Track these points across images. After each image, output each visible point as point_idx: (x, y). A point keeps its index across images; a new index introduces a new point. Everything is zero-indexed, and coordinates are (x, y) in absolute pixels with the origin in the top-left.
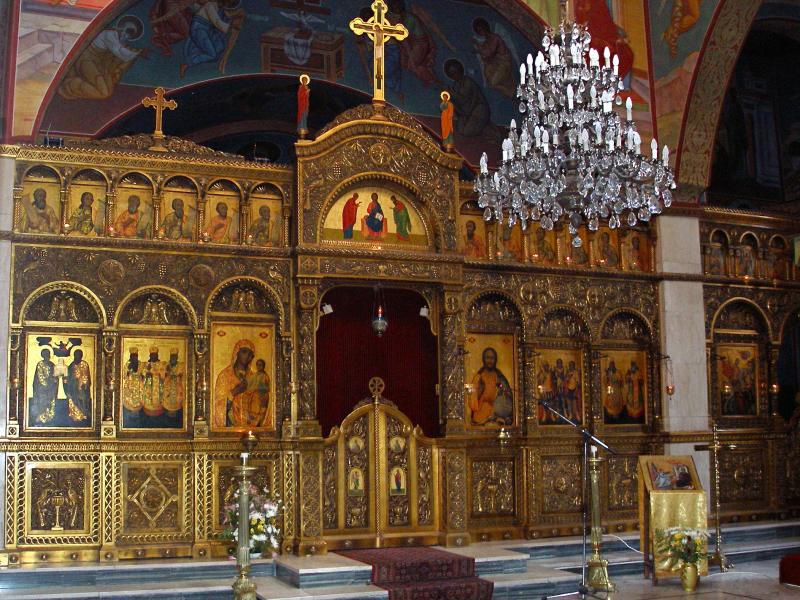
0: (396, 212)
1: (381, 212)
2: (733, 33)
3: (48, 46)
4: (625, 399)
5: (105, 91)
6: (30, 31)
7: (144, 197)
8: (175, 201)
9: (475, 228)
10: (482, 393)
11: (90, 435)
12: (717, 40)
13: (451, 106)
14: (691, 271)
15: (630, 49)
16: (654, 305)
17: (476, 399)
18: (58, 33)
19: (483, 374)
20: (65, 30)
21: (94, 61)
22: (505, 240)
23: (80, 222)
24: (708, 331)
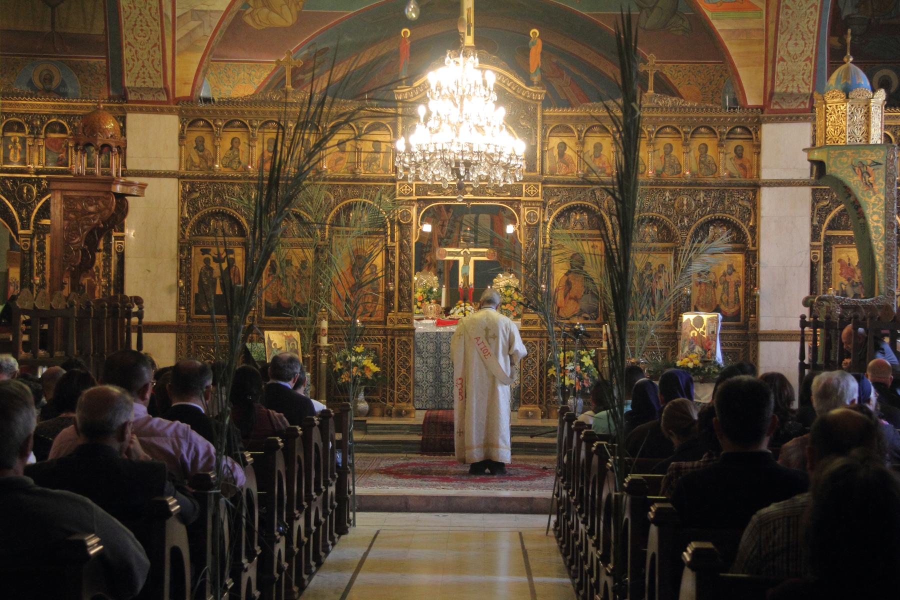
3: (200, 22)
4: (718, 299)
6: (186, 11)
7: (244, 140)
10: (569, 291)
13: (539, 42)
14: (796, 176)
16: (754, 208)
17: (563, 297)
18: (206, 11)
19: (570, 276)
20: (212, 8)
22: (595, 157)
24: (815, 236)
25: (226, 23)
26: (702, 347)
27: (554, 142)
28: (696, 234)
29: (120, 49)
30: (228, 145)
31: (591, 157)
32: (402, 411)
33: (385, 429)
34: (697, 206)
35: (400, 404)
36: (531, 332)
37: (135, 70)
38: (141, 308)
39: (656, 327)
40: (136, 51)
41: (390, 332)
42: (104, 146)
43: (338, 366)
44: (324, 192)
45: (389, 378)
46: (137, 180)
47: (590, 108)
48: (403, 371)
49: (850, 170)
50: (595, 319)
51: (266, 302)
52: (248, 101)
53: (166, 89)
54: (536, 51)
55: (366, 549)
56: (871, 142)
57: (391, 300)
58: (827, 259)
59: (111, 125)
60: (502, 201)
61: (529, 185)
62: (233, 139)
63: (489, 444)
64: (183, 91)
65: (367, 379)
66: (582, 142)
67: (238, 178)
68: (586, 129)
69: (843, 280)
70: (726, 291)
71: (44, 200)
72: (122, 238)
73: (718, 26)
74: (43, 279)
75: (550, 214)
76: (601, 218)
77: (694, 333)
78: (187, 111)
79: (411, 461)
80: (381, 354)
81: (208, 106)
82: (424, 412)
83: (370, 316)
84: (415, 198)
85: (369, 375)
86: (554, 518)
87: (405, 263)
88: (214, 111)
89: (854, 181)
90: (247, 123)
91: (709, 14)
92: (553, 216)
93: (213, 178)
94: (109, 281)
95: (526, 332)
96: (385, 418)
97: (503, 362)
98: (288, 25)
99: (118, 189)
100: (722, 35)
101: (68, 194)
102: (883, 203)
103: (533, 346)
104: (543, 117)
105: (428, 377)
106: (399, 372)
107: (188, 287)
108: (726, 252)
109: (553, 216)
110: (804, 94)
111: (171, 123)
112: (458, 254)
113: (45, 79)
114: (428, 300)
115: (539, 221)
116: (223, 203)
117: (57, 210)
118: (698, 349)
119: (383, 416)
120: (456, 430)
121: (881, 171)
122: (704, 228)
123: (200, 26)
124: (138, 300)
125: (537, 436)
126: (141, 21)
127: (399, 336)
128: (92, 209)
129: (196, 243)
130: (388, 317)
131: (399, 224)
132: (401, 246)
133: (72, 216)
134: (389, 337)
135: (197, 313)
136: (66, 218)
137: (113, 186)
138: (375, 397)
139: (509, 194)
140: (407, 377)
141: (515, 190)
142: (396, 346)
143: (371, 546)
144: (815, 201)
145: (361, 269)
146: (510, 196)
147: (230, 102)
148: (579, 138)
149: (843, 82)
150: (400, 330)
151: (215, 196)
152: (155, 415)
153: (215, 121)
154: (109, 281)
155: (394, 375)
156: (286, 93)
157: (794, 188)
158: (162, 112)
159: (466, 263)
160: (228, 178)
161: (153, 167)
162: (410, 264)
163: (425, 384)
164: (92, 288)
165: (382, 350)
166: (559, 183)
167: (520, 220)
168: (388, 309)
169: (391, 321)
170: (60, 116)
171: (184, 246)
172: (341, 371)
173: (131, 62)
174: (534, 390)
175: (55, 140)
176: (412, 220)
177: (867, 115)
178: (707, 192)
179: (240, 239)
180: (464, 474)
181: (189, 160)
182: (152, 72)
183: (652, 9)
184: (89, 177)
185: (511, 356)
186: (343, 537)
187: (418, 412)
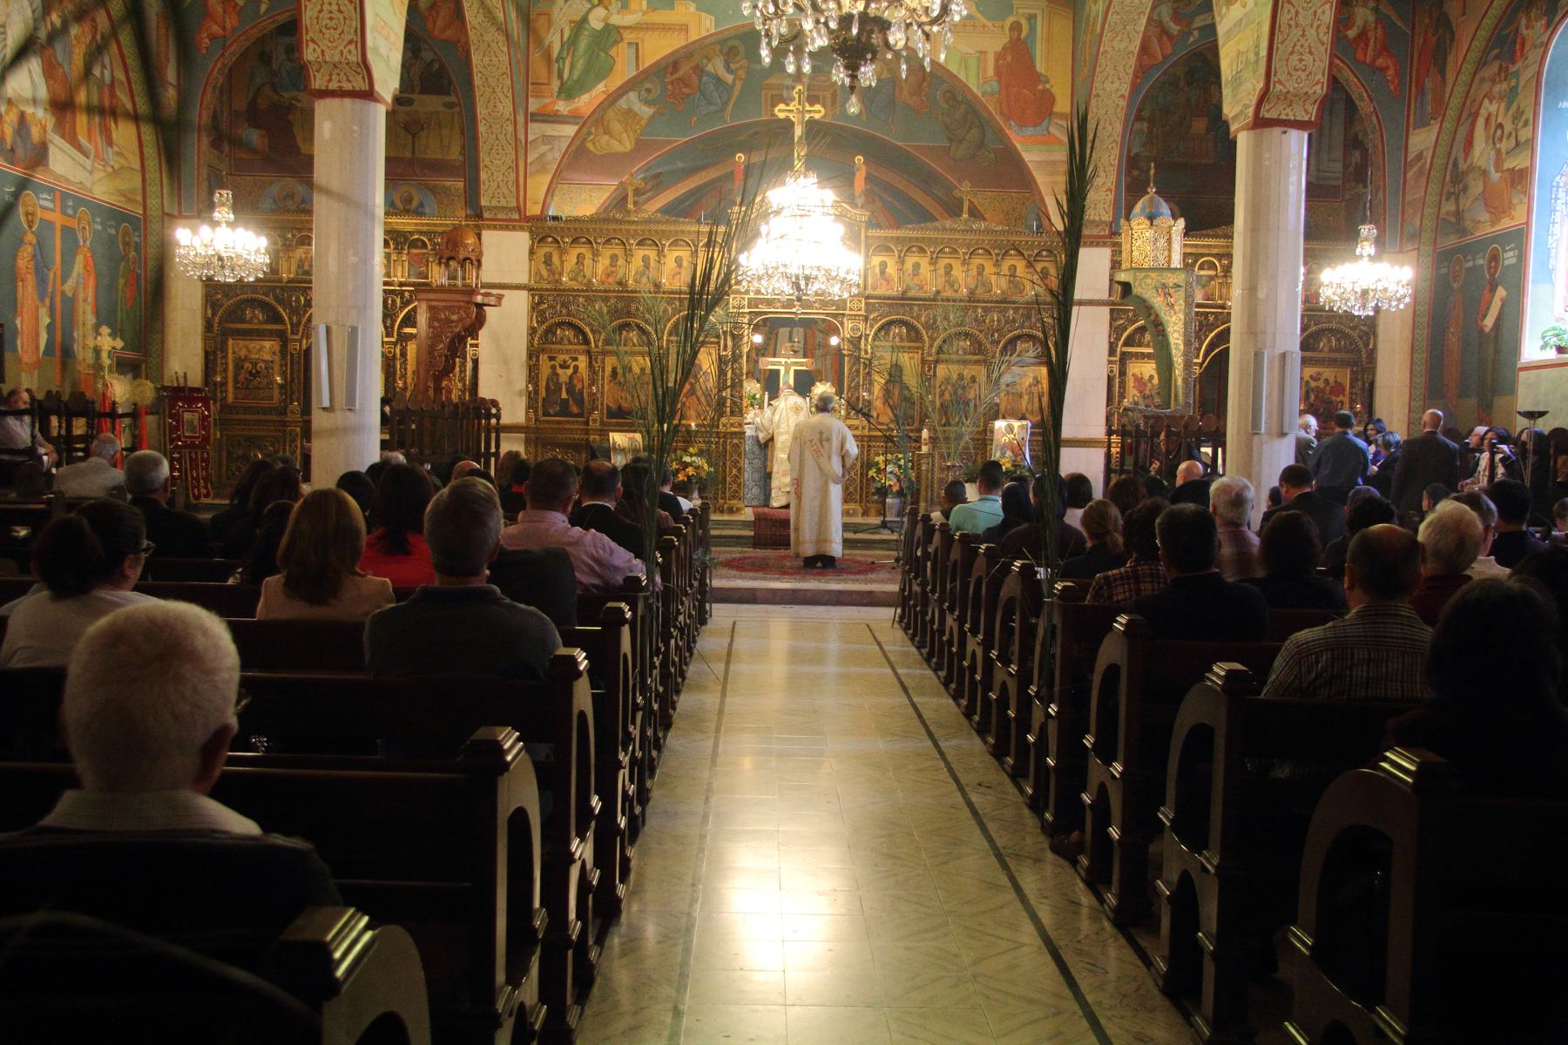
2: (1116, 85)
4: (1024, 408)
5: (627, 145)
7: (589, 255)
8: (644, 256)
11: (581, 423)
12: (1101, 93)
15: (1051, 93)
20: (560, 134)
21: (619, 121)
23: (577, 275)
24: (1112, 352)
25: (574, 148)
26: (1013, 452)
27: (876, 260)
28: (1005, 348)
29: (478, 171)
30: (574, 260)
34: (1007, 322)
37: (490, 192)
38: (499, 410)
39: (971, 433)
40: (1297, 13)
41: (722, 435)
42: (465, 259)
44: (664, 304)
46: (494, 292)
47: (910, 230)
48: (734, 471)
49: (1154, 291)
51: (608, 406)
52: (592, 219)
53: (518, 208)
54: (860, 177)
55: (728, 640)
56: (1172, 266)
58: (1123, 373)
59: (471, 241)
60: (827, 314)
62: (579, 255)
63: (822, 538)
64: (534, 209)
65: (701, 478)
66: (902, 261)
67: (582, 291)
69: (1136, 392)
70: (1031, 400)
71: (407, 310)
72: (477, 346)
73: (1026, 156)
74: (405, 383)
75: (872, 327)
76: (917, 332)
77: (1005, 439)
78: (537, 228)
79: (746, 555)
81: (555, 223)
84: (747, 310)
85: (703, 475)
86: (899, 611)
88: (562, 229)
89: (1157, 302)
90: (592, 239)
91: (1019, 146)
93: (560, 290)
94: (464, 385)
97: (836, 466)
98: (627, 151)
99: (479, 299)
100: (1030, 165)
101: (434, 303)
102: (1182, 322)
104: (866, 237)
106: (731, 473)
107: (536, 392)
108: (1034, 364)
110: (1105, 222)
111: (522, 239)
112: (779, 363)
113: (406, 200)
114: (752, 405)
116: (569, 314)
117: (422, 318)
118: (1009, 454)
120: (792, 527)
121: (1182, 293)
122: (1012, 342)
123: (550, 150)
124: (494, 403)
126: (1302, 46)
128: (454, 317)
129: (543, 351)
133: (436, 324)
135: (544, 415)
136: (430, 326)
137: (474, 297)
141: (841, 304)
143: (732, 636)
144: (1112, 319)
147: (577, 220)
148: (900, 257)
149: (1147, 210)
151: (561, 307)
152: (573, 525)
153: (562, 237)
154: (464, 385)
156: (628, 212)
157: (1095, 308)
158: (514, 229)
159: (787, 372)
160: (574, 290)
161: (505, 281)
164: (449, 392)
166: (880, 298)
168: (722, 414)
170: (421, 233)
171: (533, 354)
173: (487, 183)
175: (416, 255)
177: (1169, 241)
178: (1016, 310)
179: (584, 347)
180: (799, 568)
181: (538, 273)
182: (506, 192)
183: (961, 142)
184: (451, 290)
185: (843, 457)
186: (704, 628)
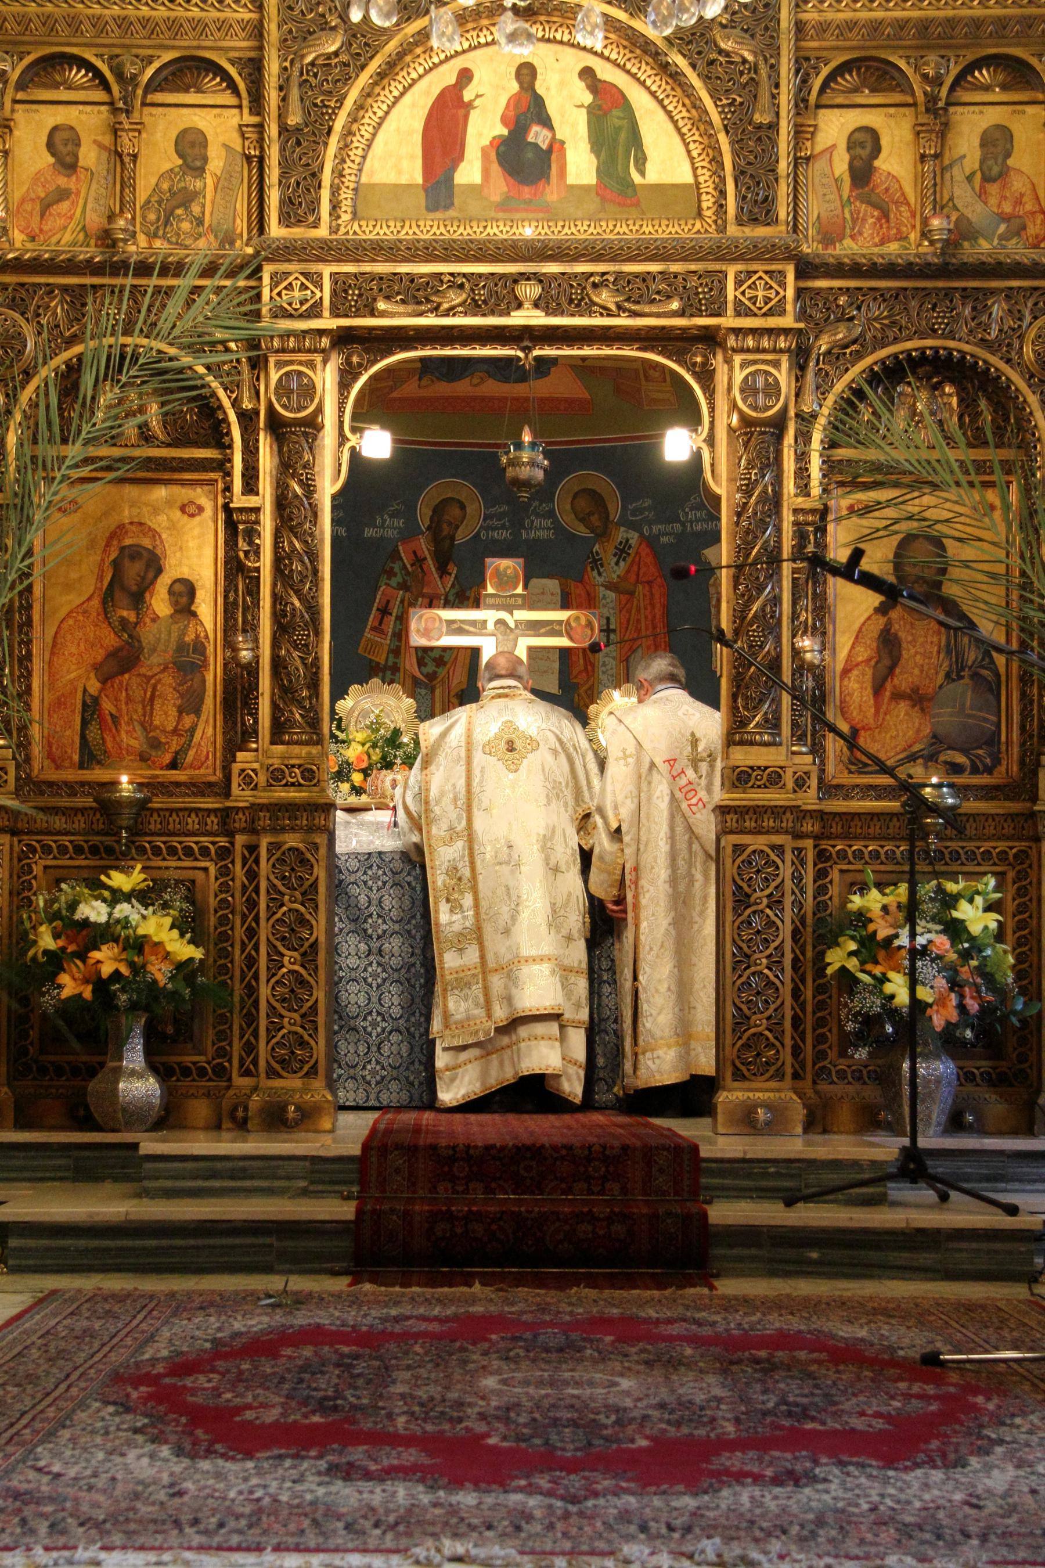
0: (597, 115)
1: (546, 122)
9: (877, 150)
10: (891, 670)
19: (895, 614)
22: (987, 179)
31: (969, 179)
32: (283, 1109)
33: (214, 1175)
35: (278, 1083)
36: (759, 811)
41: (240, 820)
43: (47, 941)
45: (238, 989)
48: (290, 961)
50: (989, 770)
57: (246, 704)
61: (750, 274)
68: (955, 70)
75: (822, 390)
80: (213, 902)
82: (369, 1118)
83: (173, 765)
85: (160, 972)
87: (297, 566)
92: (831, 399)
95: (741, 811)
96: (225, 1135)
103: (769, 863)
105: (386, 1000)
109: (831, 399)
115: (785, 409)
119: (218, 1127)
125: (807, 1199)
127: (274, 830)
130: (236, 768)
131: (276, 425)
132: (282, 503)
134: (240, 839)
138: (188, 1059)
139: (675, 305)
140: (302, 982)
142: (264, 867)
145: (139, 598)
146: (681, 313)
150: (276, 809)
155: (256, 977)
162: (316, 572)
163: (375, 1024)
165: (214, 886)
166: (855, 270)
167: (712, 409)
169: (247, 781)
172: (55, 961)
174: (775, 1026)
176: (320, 410)
187: (347, 1118)
